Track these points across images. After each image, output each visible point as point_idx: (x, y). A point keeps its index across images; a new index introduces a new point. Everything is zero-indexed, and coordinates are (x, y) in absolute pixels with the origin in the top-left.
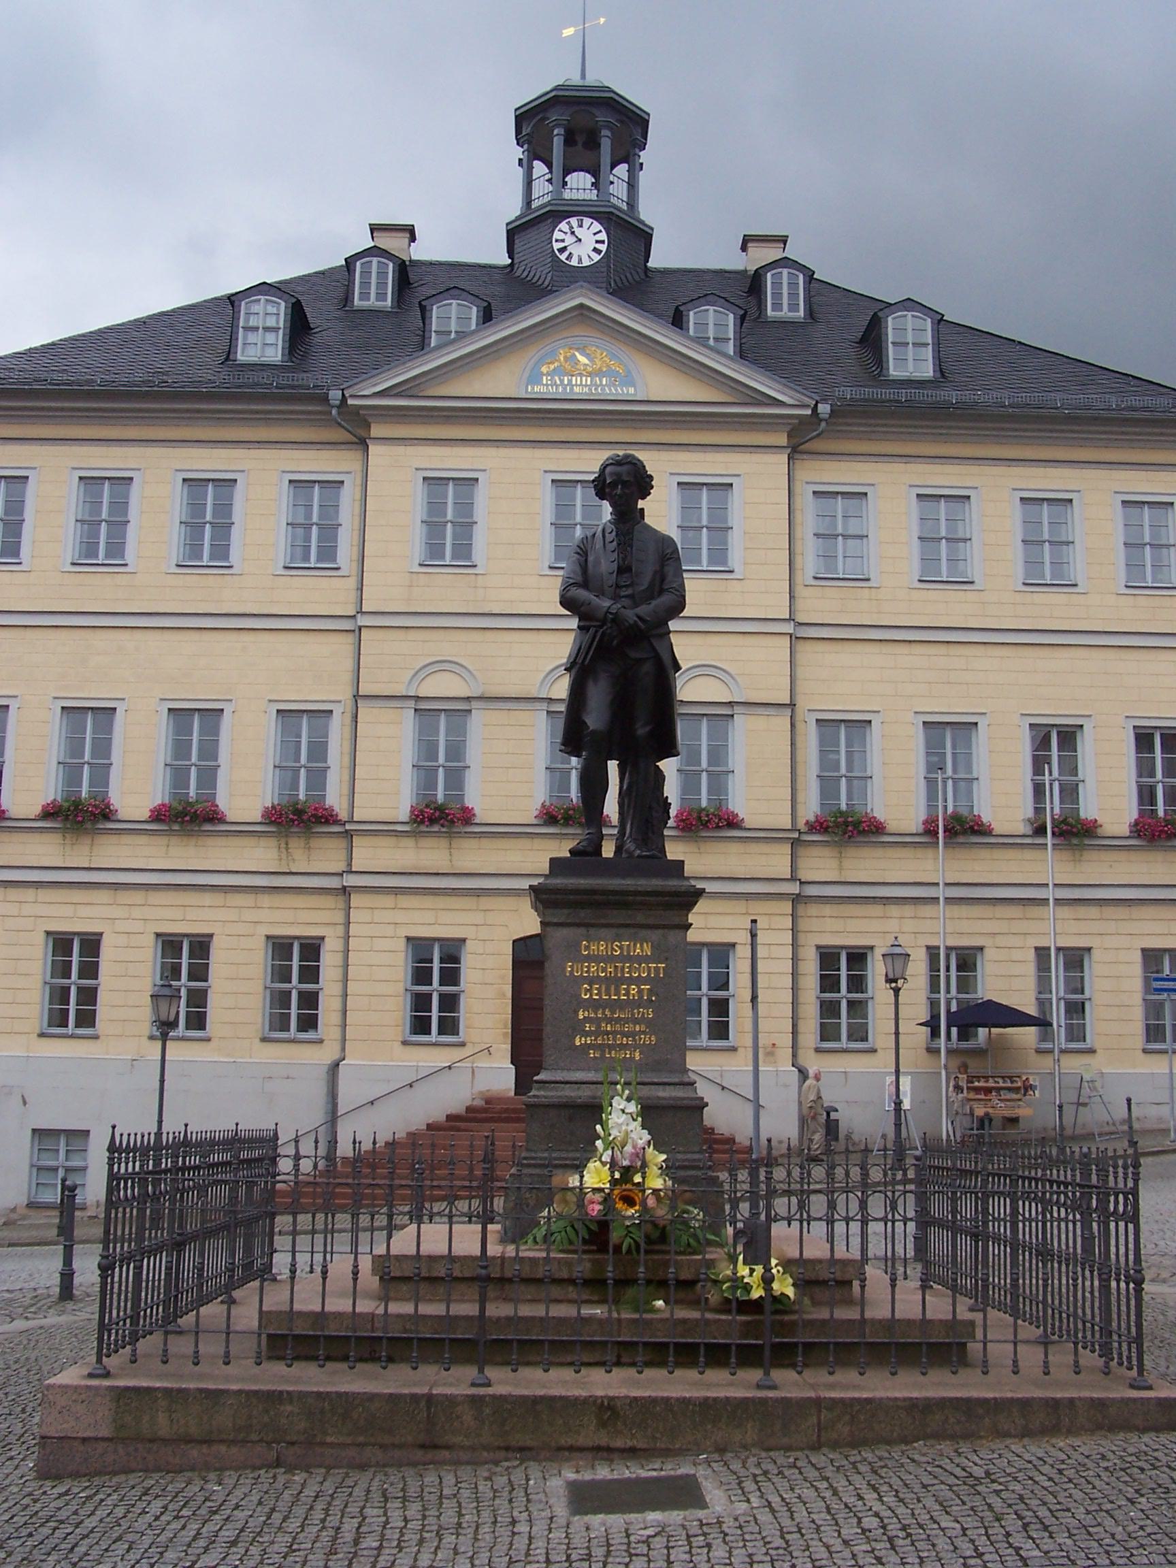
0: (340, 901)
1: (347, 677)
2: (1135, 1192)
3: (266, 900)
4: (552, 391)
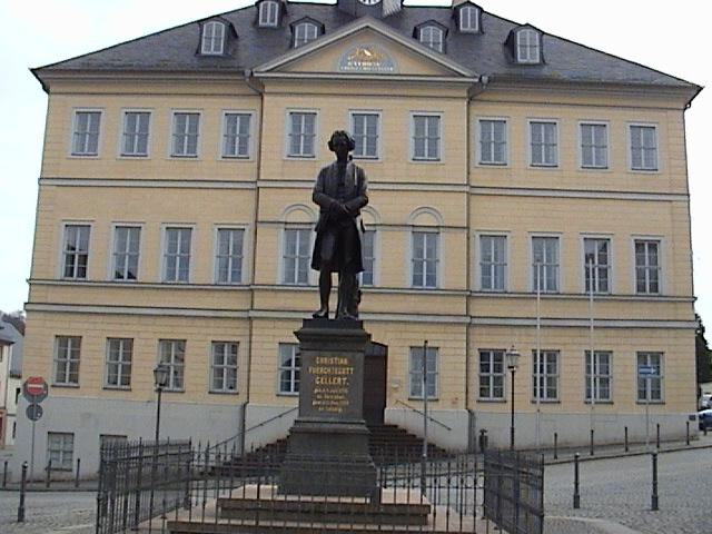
0: (247, 325)
1: (252, 213)
2: (542, 477)
3: (212, 323)
4: (356, 70)
